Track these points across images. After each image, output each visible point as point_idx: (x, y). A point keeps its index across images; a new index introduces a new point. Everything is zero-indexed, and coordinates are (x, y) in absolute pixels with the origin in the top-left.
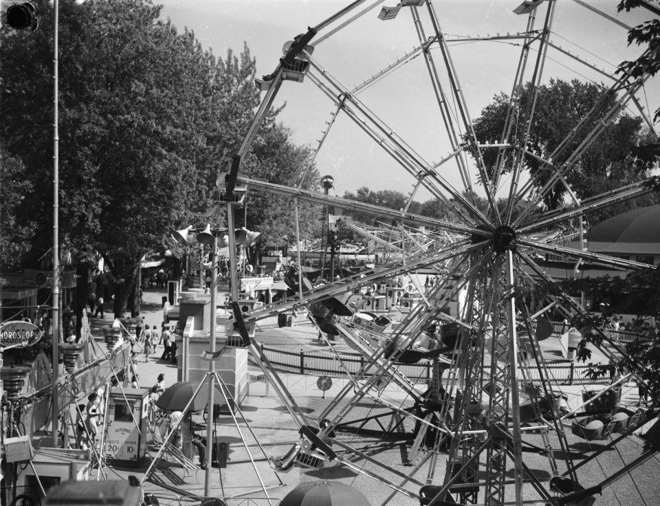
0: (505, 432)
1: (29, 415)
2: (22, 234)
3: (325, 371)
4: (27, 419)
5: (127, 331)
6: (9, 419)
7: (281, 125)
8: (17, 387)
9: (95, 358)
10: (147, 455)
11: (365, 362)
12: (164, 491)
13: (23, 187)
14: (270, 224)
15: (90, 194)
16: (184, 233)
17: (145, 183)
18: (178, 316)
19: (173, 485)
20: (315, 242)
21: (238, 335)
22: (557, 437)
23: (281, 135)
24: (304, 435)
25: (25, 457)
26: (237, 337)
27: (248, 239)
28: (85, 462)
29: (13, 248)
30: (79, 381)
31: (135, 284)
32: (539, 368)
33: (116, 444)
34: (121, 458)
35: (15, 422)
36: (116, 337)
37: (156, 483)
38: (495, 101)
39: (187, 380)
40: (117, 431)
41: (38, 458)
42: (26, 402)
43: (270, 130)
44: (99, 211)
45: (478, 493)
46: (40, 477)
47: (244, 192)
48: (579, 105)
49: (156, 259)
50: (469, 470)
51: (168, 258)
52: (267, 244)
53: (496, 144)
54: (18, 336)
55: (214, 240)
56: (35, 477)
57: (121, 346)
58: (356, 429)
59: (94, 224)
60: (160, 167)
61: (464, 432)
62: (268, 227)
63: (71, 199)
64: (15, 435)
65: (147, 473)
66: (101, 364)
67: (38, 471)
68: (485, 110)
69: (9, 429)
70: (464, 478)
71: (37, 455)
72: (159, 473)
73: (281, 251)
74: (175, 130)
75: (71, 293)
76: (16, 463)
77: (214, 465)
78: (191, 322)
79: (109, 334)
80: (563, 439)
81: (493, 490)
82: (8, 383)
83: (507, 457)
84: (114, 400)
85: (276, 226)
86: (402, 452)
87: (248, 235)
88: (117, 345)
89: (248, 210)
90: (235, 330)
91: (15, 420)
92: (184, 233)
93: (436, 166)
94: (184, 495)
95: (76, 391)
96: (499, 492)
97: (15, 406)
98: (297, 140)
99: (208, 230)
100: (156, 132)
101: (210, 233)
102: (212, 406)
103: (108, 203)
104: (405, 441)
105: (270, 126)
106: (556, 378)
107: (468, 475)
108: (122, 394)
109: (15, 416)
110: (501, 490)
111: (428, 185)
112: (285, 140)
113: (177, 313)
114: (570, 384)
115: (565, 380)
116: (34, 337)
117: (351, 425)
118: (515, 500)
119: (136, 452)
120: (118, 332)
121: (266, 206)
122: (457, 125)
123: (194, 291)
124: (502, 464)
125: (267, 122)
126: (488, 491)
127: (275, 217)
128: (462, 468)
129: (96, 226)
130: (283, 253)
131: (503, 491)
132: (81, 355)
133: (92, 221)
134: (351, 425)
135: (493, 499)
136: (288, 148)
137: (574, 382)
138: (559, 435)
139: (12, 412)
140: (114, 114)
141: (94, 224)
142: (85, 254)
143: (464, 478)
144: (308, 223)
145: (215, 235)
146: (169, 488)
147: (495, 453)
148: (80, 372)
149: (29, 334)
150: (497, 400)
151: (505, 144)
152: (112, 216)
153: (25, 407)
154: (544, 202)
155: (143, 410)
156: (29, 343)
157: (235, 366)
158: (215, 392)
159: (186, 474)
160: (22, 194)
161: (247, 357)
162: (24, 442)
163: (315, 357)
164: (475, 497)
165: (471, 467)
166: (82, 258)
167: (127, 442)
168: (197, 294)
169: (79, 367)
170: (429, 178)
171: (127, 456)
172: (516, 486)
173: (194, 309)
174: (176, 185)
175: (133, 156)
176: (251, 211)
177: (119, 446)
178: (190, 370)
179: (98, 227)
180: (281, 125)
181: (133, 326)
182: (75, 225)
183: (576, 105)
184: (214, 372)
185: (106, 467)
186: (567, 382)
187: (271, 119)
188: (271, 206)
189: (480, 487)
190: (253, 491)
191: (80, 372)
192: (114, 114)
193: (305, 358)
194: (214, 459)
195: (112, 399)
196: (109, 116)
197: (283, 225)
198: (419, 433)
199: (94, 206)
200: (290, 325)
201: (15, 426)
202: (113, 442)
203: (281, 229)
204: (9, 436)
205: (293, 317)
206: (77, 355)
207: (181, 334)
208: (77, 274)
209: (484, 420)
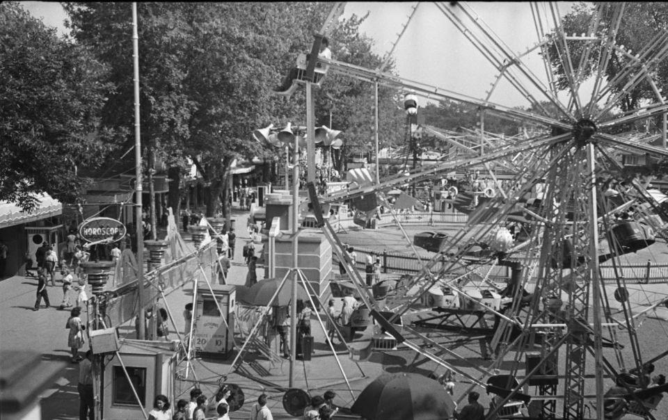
0: (585, 326)
1: (115, 308)
2: (108, 135)
3: (407, 270)
4: (113, 312)
5: (214, 230)
6: (94, 311)
7: (365, 35)
8: (101, 281)
9: (182, 255)
10: (235, 348)
11: (446, 261)
12: (251, 382)
13: (107, 88)
14: (355, 131)
15: (179, 100)
16: (265, 132)
17: (230, 89)
18: (264, 217)
19: (260, 377)
20: (399, 150)
21: (313, 216)
22: (628, 334)
23: (364, 45)
24: (376, 321)
25: (112, 349)
26: (312, 218)
27: (328, 138)
28: (171, 353)
29: (97, 147)
30: (167, 277)
31: (225, 187)
32: (615, 267)
33: (205, 338)
34: (209, 351)
35: (101, 315)
36: (203, 235)
37: (243, 374)
38: (574, 10)
39: (274, 276)
40: (205, 325)
41: (125, 349)
42: (112, 296)
43: (353, 39)
44: (187, 116)
45: (558, 386)
46: (127, 368)
47: (323, 75)
48: (656, 13)
49: (246, 165)
50: (548, 363)
51: (257, 165)
52: (352, 150)
53: (583, 37)
54: (102, 232)
55: (294, 139)
56: (121, 367)
57: (208, 244)
58: (436, 325)
59: (183, 129)
60: (244, 74)
61: (533, 325)
62: (352, 134)
63: (160, 105)
64: (101, 327)
65: (233, 364)
66: (189, 260)
67: (124, 363)
68: (563, 19)
69: (95, 322)
70: (544, 371)
71: (124, 346)
72: (245, 365)
73: (366, 158)
74: (258, 37)
75: (166, 197)
76: (103, 355)
77: (298, 358)
78: (276, 222)
79: (196, 233)
80: (633, 336)
81: (573, 383)
82: (93, 277)
83: (588, 353)
84: (203, 296)
85: (361, 133)
86: (481, 347)
87: (329, 133)
88: (203, 244)
89: (333, 117)
90: (309, 210)
91: (100, 313)
92: (265, 132)
93: (521, 56)
94: (269, 386)
95: (163, 286)
96: (579, 386)
97: (100, 299)
98: (378, 50)
99: (288, 129)
100: (240, 39)
101: (290, 131)
102: (295, 301)
103: (197, 109)
104: (484, 337)
105: (353, 36)
106: (638, 277)
107: (547, 368)
108: (209, 290)
109: (100, 308)
110: (581, 384)
111: (511, 79)
112: (368, 50)
113: (261, 214)
114: (646, 283)
115: (642, 279)
116: (118, 233)
117: (429, 322)
118: (594, 394)
119: (224, 346)
120: (205, 231)
121: (351, 114)
122: (544, 16)
123: (279, 193)
124: (582, 357)
125: (351, 31)
126: (567, 384)
127: (360, 125)
128: (541, 362)
129: (185, 131)
130: (368, 159)
131: (583, 384)
132: (168, 251)
133: (181, 126)
134: (429, 322)
135: (574, 392)
136: (371, 57)
137: (650, 281)
138: (630, 331)
139: (98, 305)
140: (199, 21)
141: (183, 129)
142: (175, 159)
143: (544, 371)
144: (392, 131)
145: (295, 134)
146: (254, 379)
147: (575, 346)
148: (168, 268)
149: (114, 230)
150: (577, 294)
151: (593, 37)
152: (200, 120)
153: (111, 301)
154: (621, 108)
155: (230, 306)
156: (114, 239)
157: (319, 264)
158: (298, 288)
159: (272, 367)
160: (106, 96)
161: (331, 257)
162: (110, 334)
163: (398, 257)
164: (554, 390)
165: (549, 361)
166: (172, 163)
167: (215, 336)
168: (281, 195)
169: (166, 262)
170: (513, 69)
171: (216, 349)
172: (597, 380)
173: (279, 210)
174: (260, 89)
175: (219, 63)
176: (336, 119)
177: (208, 339)
178: (276, 269)
179: (188, 132)
180: (365, 35)
181: (220, 225)
182: (164, 130)
183: (653, 13)
184: (296, 268)
185: (195, 359)
186: (644, 281)
187: (354, 28)
188: (355, 114)
189: (560, 380)
190: (336, 383)
191: (168, 268)
192: (199, 21)
193: (388, 258)
194: (297, 353)
195: (200, 294)
196: (194, 23)
197: (367, 132)
198: (499, 328)
199: (182, 111)
200: (374, 228)
201: (101, 319)
202: (201, 335)
203: (365, 136)
204: (95, 329)
205: (377, 220)
206: (162, 252)
207: (268, 234)
208: (169, 178)
209: (563, 314)
